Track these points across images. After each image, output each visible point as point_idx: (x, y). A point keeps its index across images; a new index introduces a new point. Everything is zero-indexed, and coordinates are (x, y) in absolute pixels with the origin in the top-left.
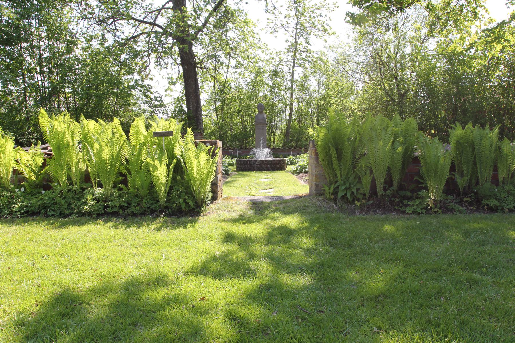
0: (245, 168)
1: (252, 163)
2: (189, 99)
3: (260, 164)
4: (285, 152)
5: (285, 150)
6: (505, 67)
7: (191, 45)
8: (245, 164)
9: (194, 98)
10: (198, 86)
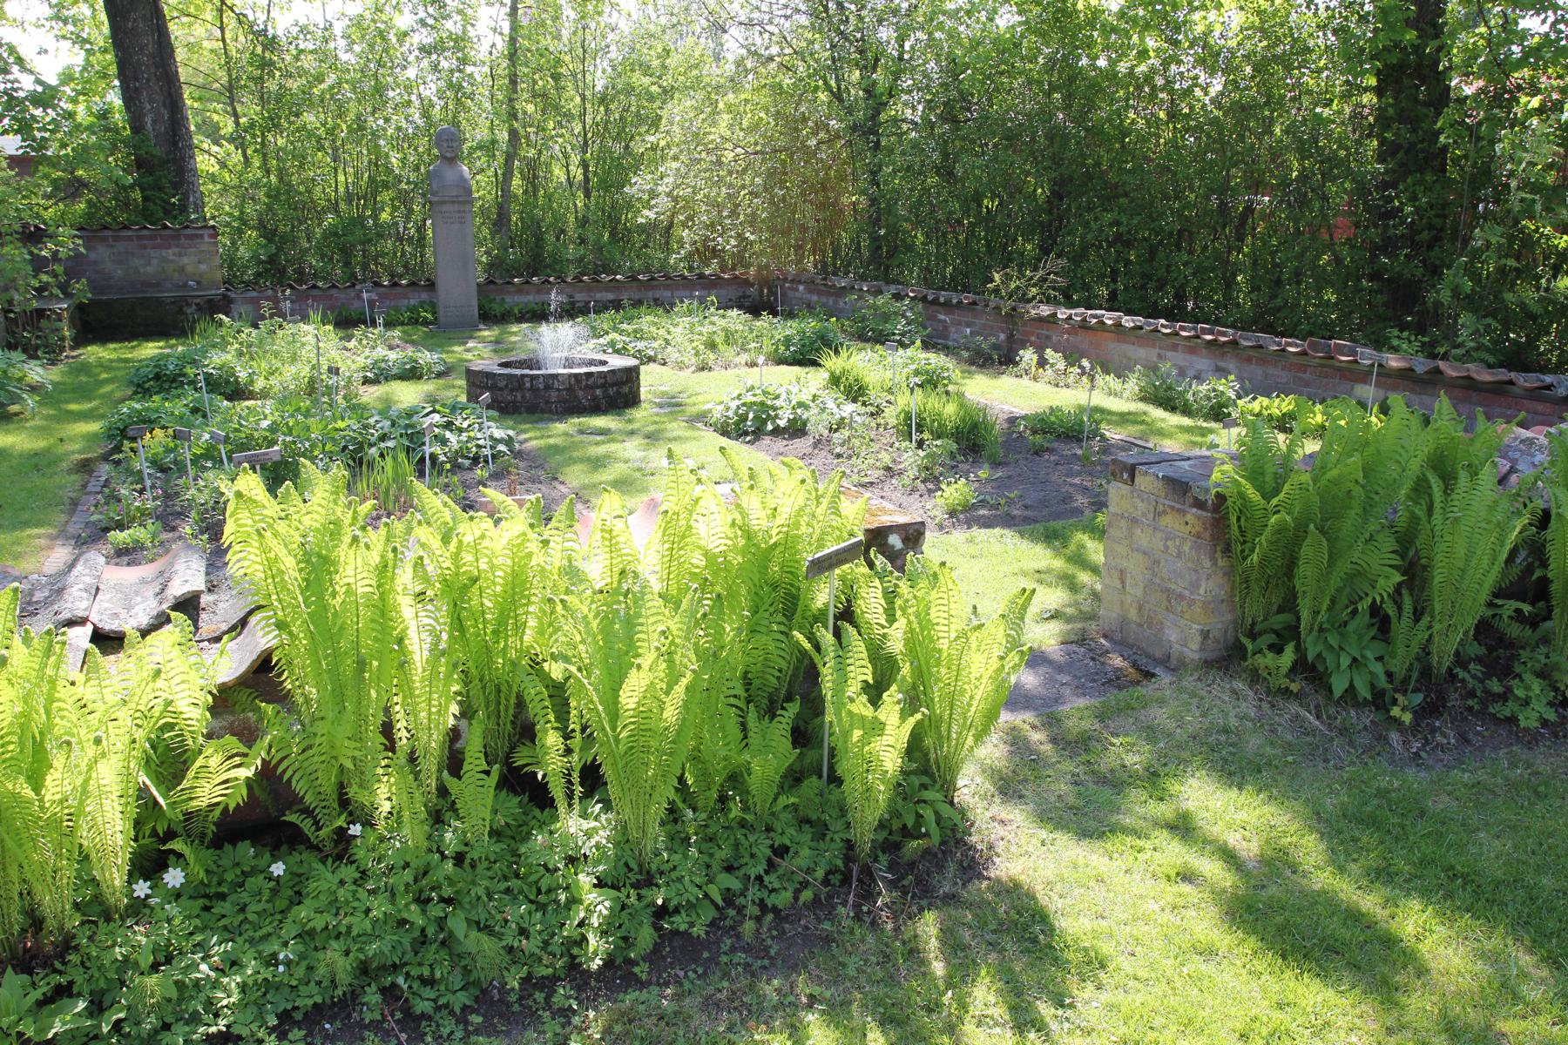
0: (514, 402)
3: (570, 389)
7: (996, 464)
8: (512, 390)
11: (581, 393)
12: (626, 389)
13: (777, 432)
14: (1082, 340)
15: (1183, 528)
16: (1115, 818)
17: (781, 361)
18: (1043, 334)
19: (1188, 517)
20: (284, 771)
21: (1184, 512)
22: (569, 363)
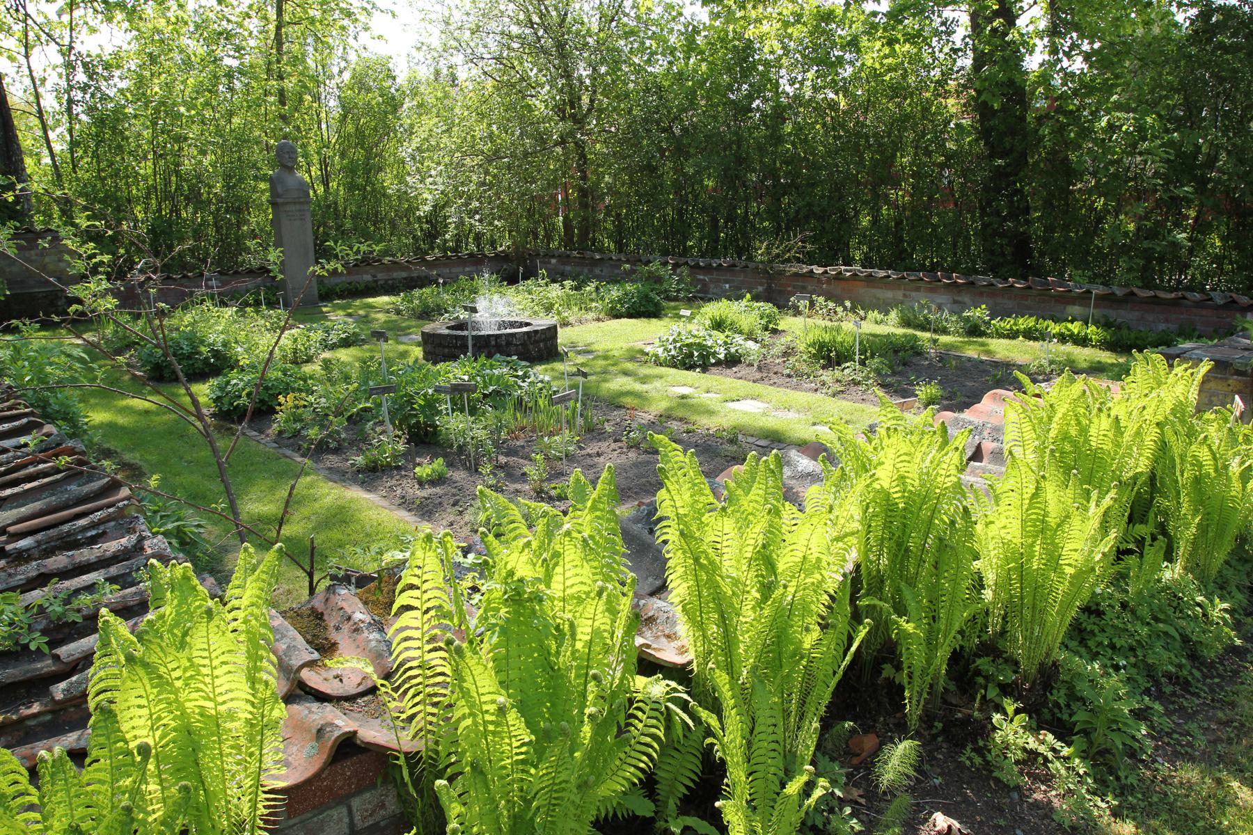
3: (524, 344)
11: (531, 347)
12: (549, 344)
13: (719, 363)
14: (837, 288)
15: (1225, 389)
16: (686, 792)
17: (618, 316)
18: (805, 284)
19: (1230, 382)
20: (693, 780)
21: (1226, 379)
22: (503, 325)
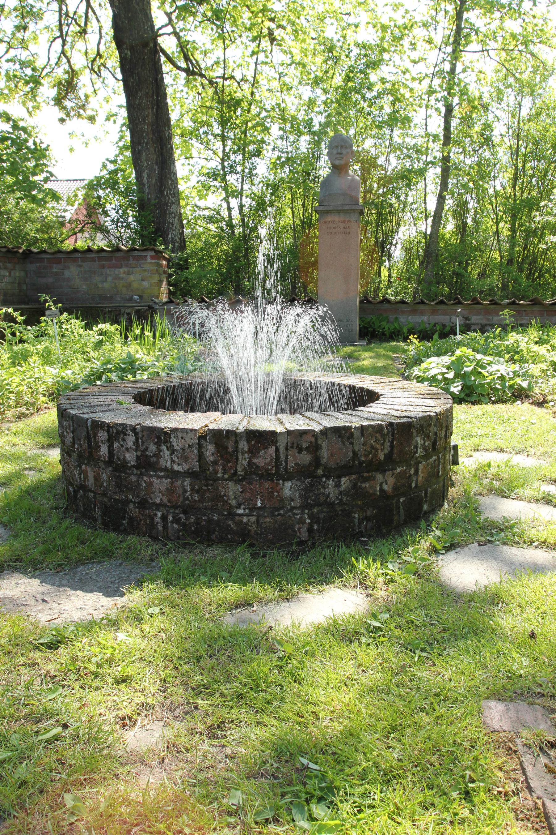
1: (131, 458)
2: (139, 152)
4: (422, 313)
5: (421, 307)
6: (125, 462)
9: (152, 149)
10: (169, 119)
